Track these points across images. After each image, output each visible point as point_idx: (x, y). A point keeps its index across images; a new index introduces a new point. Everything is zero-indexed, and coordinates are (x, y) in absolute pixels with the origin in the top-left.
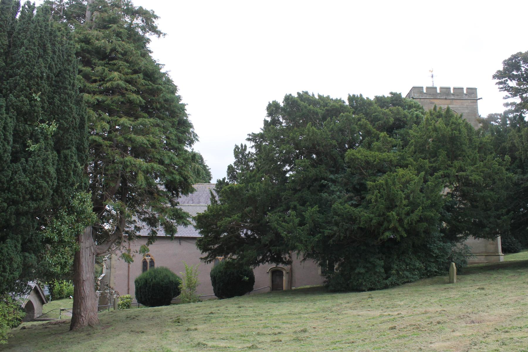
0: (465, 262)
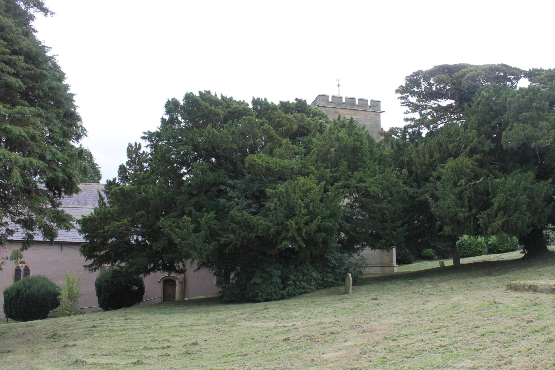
0: (361, 273)
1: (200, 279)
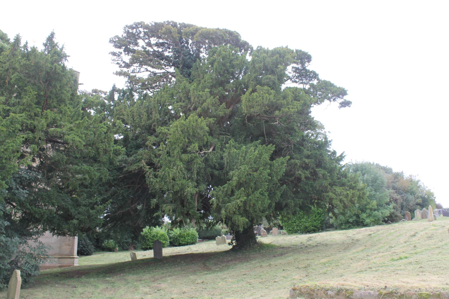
0: (37, 268)
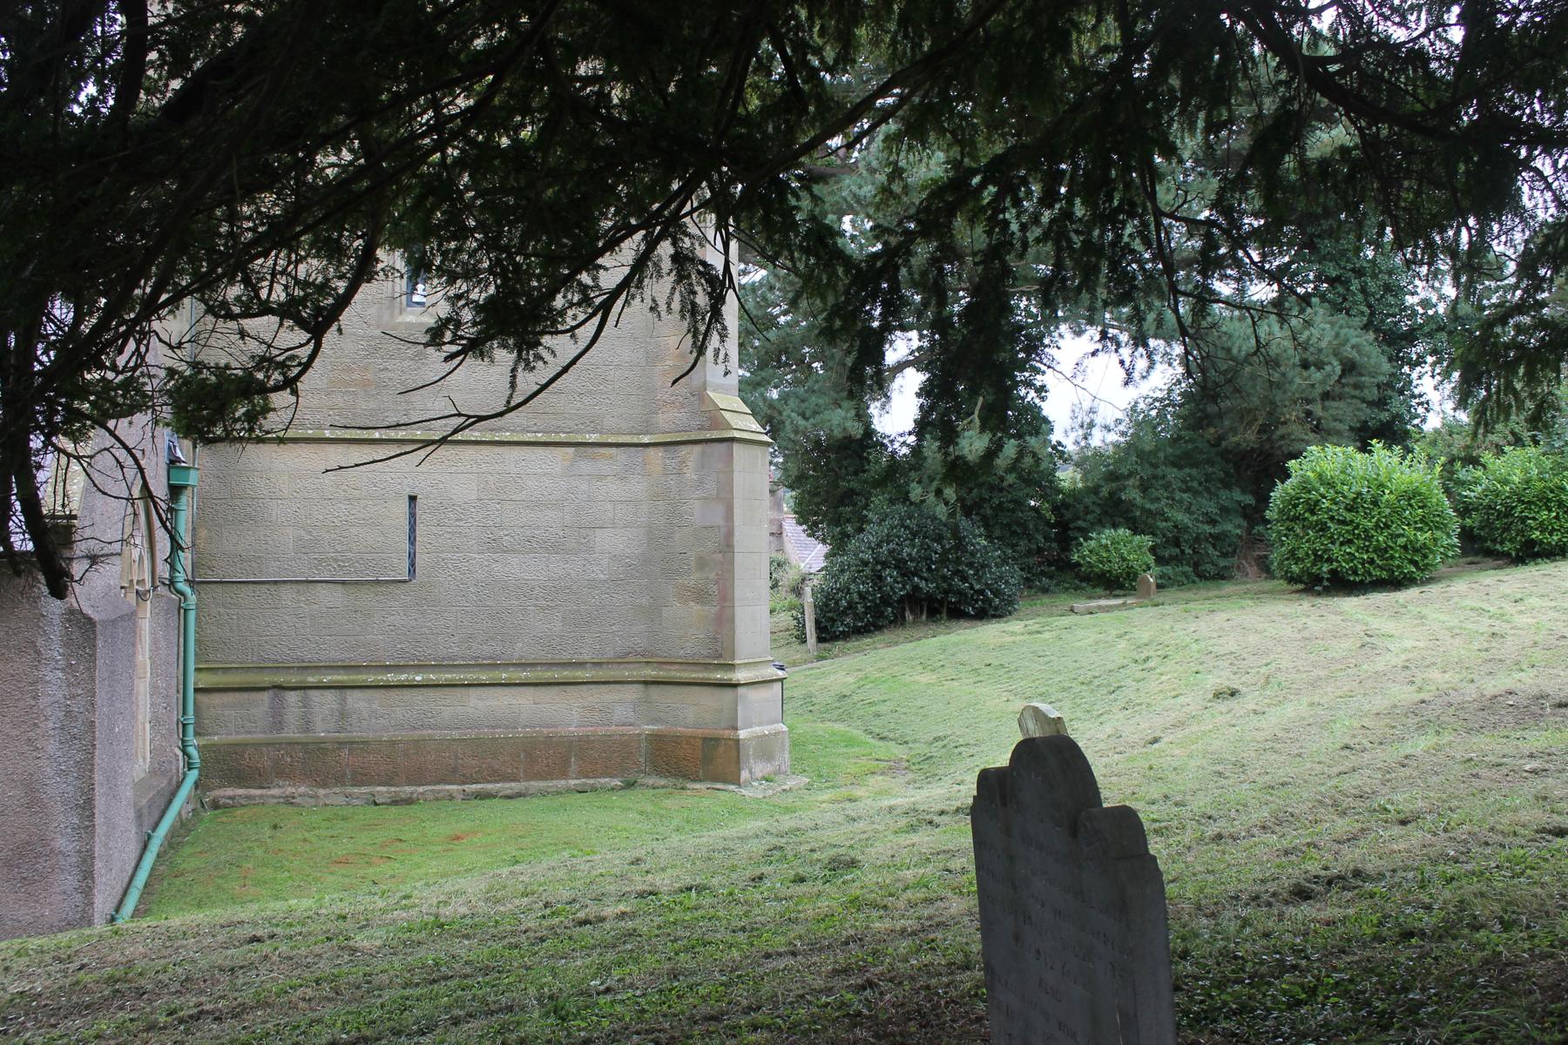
1: (944, 616)
